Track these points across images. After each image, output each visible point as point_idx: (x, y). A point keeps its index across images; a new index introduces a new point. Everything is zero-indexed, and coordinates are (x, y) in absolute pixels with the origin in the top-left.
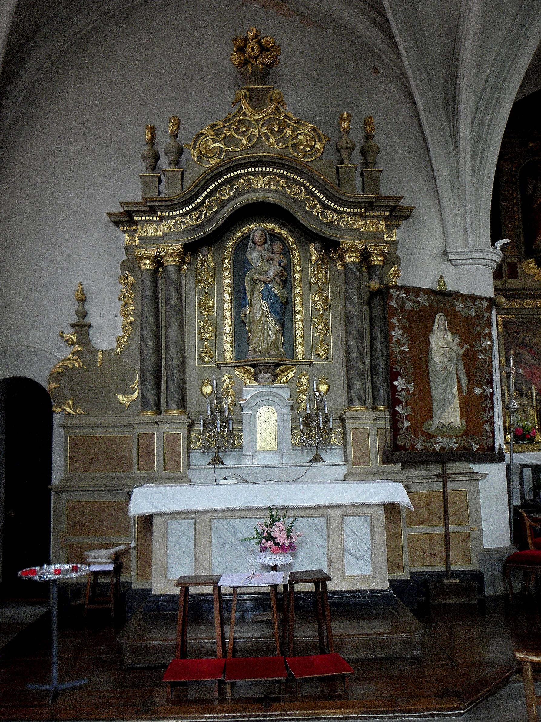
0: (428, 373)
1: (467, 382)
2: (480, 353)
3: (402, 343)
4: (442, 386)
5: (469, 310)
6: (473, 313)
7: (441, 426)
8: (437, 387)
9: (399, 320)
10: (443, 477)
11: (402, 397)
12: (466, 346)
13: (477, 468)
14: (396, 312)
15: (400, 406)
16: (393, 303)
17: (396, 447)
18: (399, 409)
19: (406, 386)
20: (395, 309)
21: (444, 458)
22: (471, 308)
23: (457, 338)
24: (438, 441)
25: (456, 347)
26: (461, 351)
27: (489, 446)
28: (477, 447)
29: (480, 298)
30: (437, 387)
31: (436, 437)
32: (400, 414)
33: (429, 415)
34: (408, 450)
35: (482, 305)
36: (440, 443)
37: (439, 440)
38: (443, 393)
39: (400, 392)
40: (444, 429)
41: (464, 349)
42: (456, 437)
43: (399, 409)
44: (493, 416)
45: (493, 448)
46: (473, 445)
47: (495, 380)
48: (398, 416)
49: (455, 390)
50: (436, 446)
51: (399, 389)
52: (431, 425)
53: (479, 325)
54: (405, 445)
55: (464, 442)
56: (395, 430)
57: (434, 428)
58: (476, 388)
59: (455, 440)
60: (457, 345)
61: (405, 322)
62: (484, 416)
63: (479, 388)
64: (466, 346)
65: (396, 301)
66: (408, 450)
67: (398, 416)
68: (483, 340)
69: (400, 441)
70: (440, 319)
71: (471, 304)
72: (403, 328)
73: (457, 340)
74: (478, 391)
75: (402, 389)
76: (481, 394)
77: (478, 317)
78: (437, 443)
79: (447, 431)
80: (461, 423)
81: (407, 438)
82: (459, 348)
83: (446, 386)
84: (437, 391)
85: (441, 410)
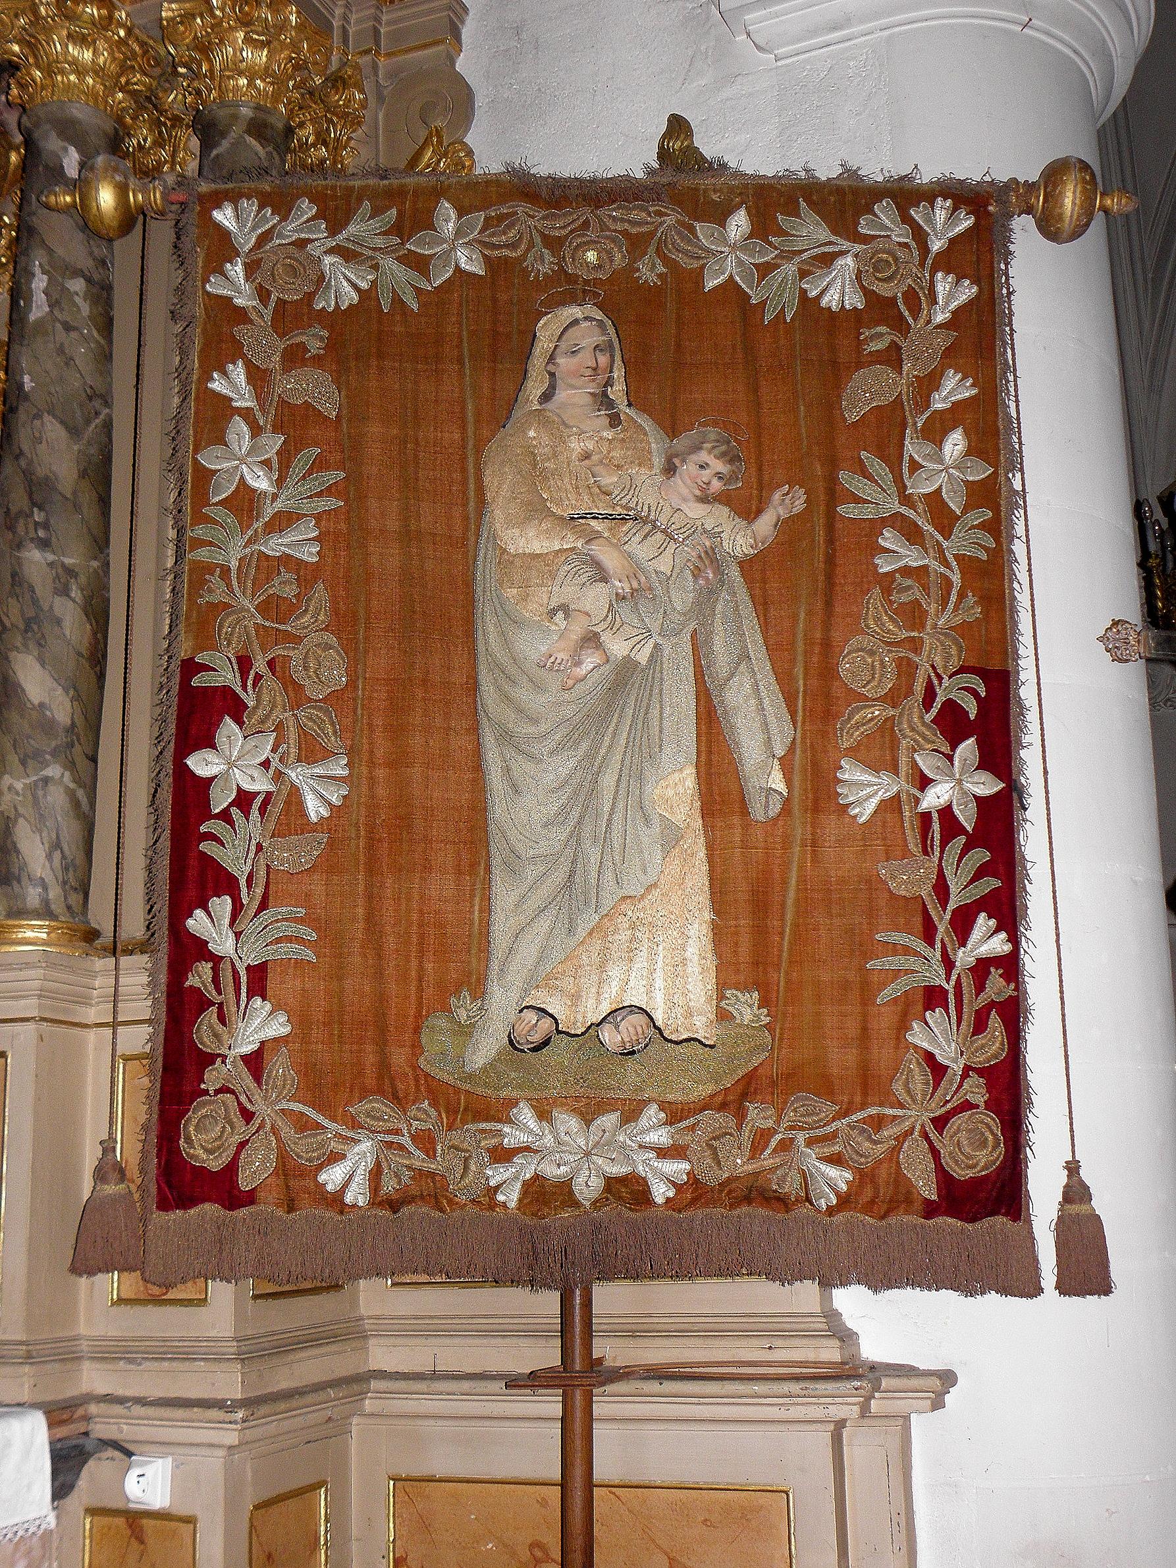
0: (473, 687)
1: (782, 734)
2: (889, 539)
3: (269, 511)
4: (564, 766)
5: (803, 274)
6: (838, 290)
7: (537, 1038)
8: (522, 767)
9: (257, 377)
10: (577, 1377)
11: (233, 851)
12: (786, 503)
13: (887, 1322)
14: (242, 332)
15: (222, 905)
16: (235, 283)
17: (180, 1182)
18: (210, 924)
19: (279, 776)
20: (241, 315)
21: (573, 1248)
22: (827, 260)
23: (704, 456)
24: (512, 1137)
25: (695, 511)
26: (741, 540)
27: (961, 1173)
28: (840, 1177)
29: (906, 195)
30: (522, 767)
31: (500, 1112)
32: (216, 960)
33: (462, 963)
34: (250, 1198)
35: (920, 236)
36: (565, 1150)
37: (526, 1124)
38: (564, 811)
39: (225, 816)
40: (560, 1051)
41: (765, 524)
42: (674, 1114)
43: (210, 924)
44: (1011, 965)
45: (1004, 1192)
46: (811, 1160)
47: (1032, 717)
48: (200, 976)
49: (676, 787)
50: (497, 1175)
51: (220, 800)
52: (465, 1032)
53: (893, 357)
54: (232, 1168)
55: (757, 1148)
56: (180, 1070)
57: (485, 1050)
58: (851, 772)
59: (661, 1137)
60: (704, 499)
61: (314, 388)
62: (912, 962)
63: (874, 767)
64: (786, 503)
65: (251, 269)
66: (250, 1198)
67: (200, 976)
68: (912, 448)
69: (205, 1141)
70: (573, 342)
71: (822, 233)
72: (294, 423)
73: (708, 466)
74: (865, 790)
75: (244, 800)
76: (892, 805)
77: (880, 309)
78: (502, 1155)
79: (590, 1069)
80: (723, 1016)
81: (248, 1116)
82: (719, 517)
83: (592, 767)
84: (527, 801)
85: (543, 925)
